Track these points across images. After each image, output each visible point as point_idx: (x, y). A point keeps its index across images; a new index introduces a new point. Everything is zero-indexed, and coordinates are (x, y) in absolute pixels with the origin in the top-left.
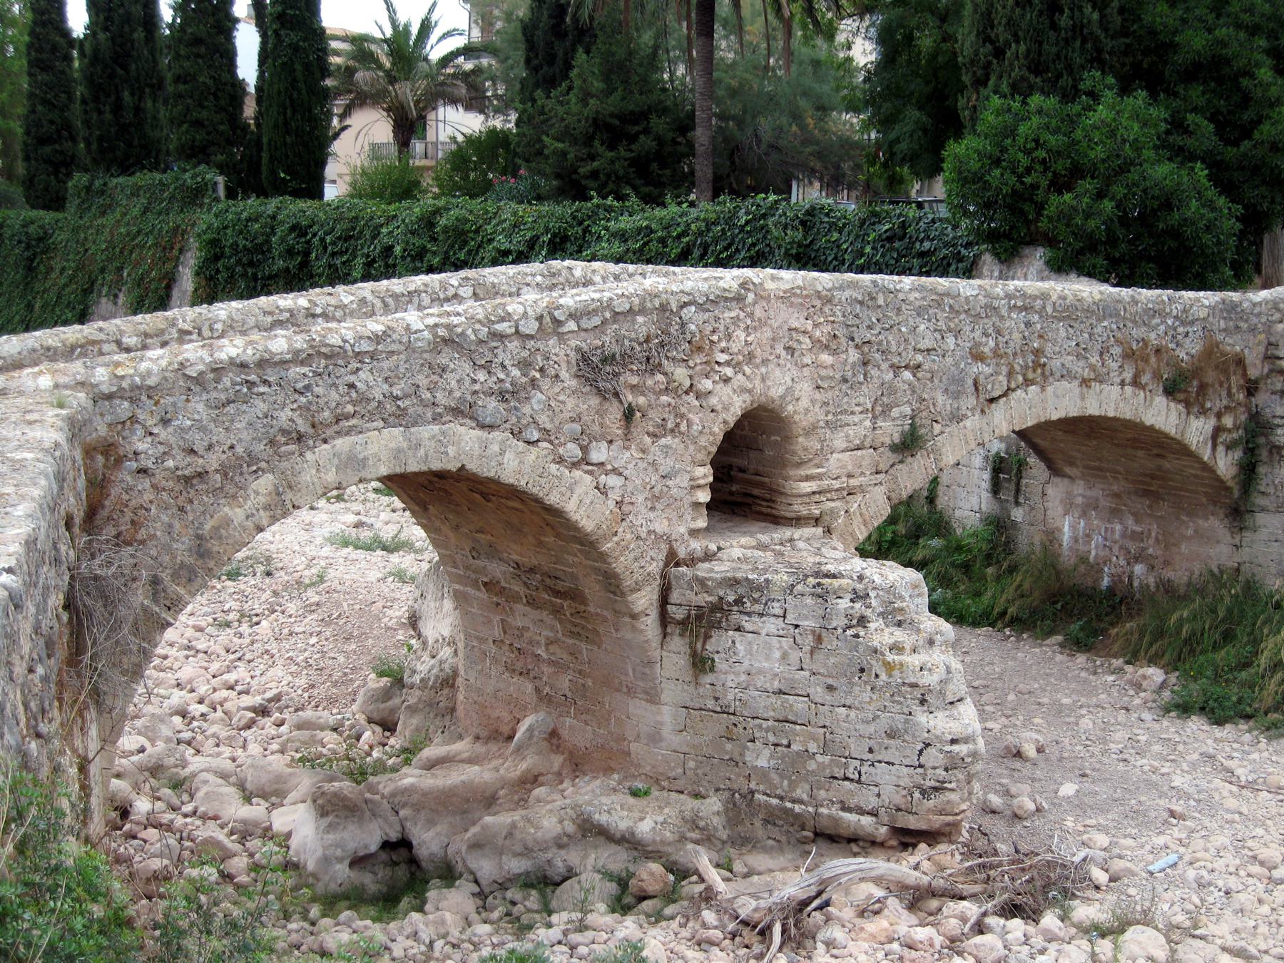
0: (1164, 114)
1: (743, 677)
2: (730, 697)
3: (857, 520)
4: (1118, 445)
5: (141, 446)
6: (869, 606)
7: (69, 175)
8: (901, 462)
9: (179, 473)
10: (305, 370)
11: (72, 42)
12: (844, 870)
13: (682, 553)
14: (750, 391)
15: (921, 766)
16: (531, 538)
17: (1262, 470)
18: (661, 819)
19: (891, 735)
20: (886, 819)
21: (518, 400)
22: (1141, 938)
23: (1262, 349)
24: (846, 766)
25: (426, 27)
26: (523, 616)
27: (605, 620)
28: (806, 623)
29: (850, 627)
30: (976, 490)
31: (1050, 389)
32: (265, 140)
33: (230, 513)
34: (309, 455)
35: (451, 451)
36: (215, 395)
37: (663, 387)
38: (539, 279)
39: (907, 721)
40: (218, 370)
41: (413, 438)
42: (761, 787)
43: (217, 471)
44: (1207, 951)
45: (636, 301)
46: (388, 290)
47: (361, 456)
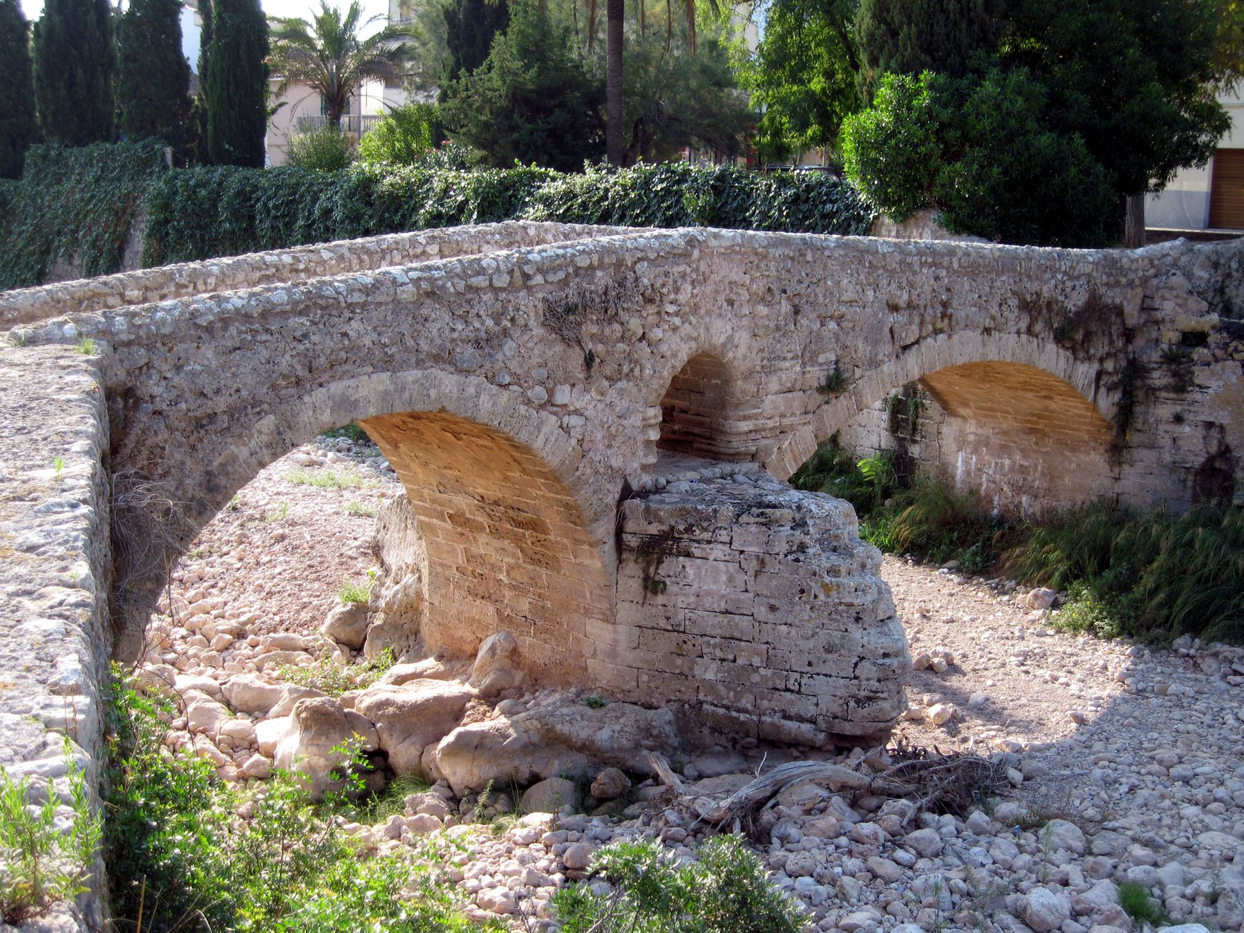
0: (1045, 90)
1: (692, 599)
2: (681, 617)
3: (788, 458)
4: (1009, 388)
5: (156, 390)
6: (807, 534)
7: (25, 147)
8: (827, 403)
9: (191, 414)
10: (303, 320)
11: (26, 25)
12: (795, 772)
13: (635, 485)
14: (695, 339)
15: (856, 678)
16: (497, 473)
17: (1138, 409)
18: (617, 728)
19: (829, 650)
20: (823, 726)
21: (492, 347)
22: (1061, 830)
23: (1138, 301)
24: (787, 678)
25: (354, 14)
26: (485, 545)
27: (565, 547)
28: (751, 549)
29: (791, 553)
30: (875, 429)
31: (956, 337)
32: (210, 114)
33: (236, 451)
34: (306, 399)
35: (433, 393)
36: (223, 343)
37: (619, 335)
38: (497, 237)
39: (843, 637)
40: (225, 320)
41: (399, 381)
42: (709, 698)
43: (224, 412)
44: (1120, 841)
46: (363, 247)
47: (353, 399)
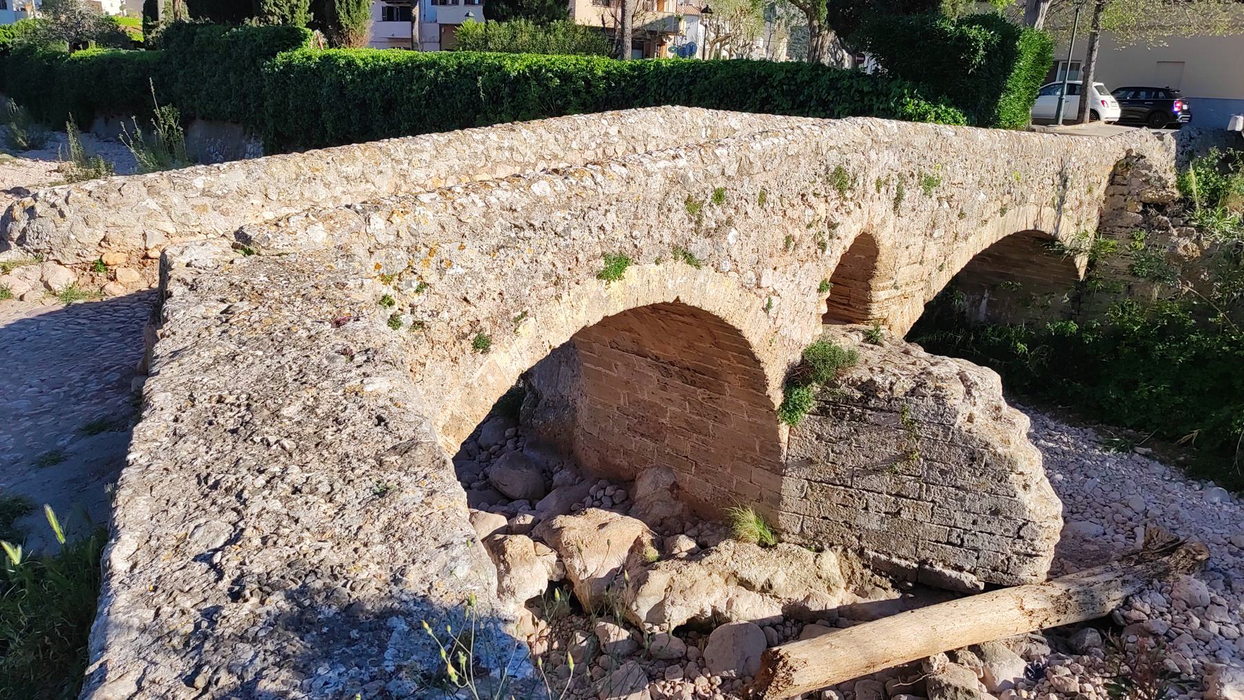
10: (565, 213)
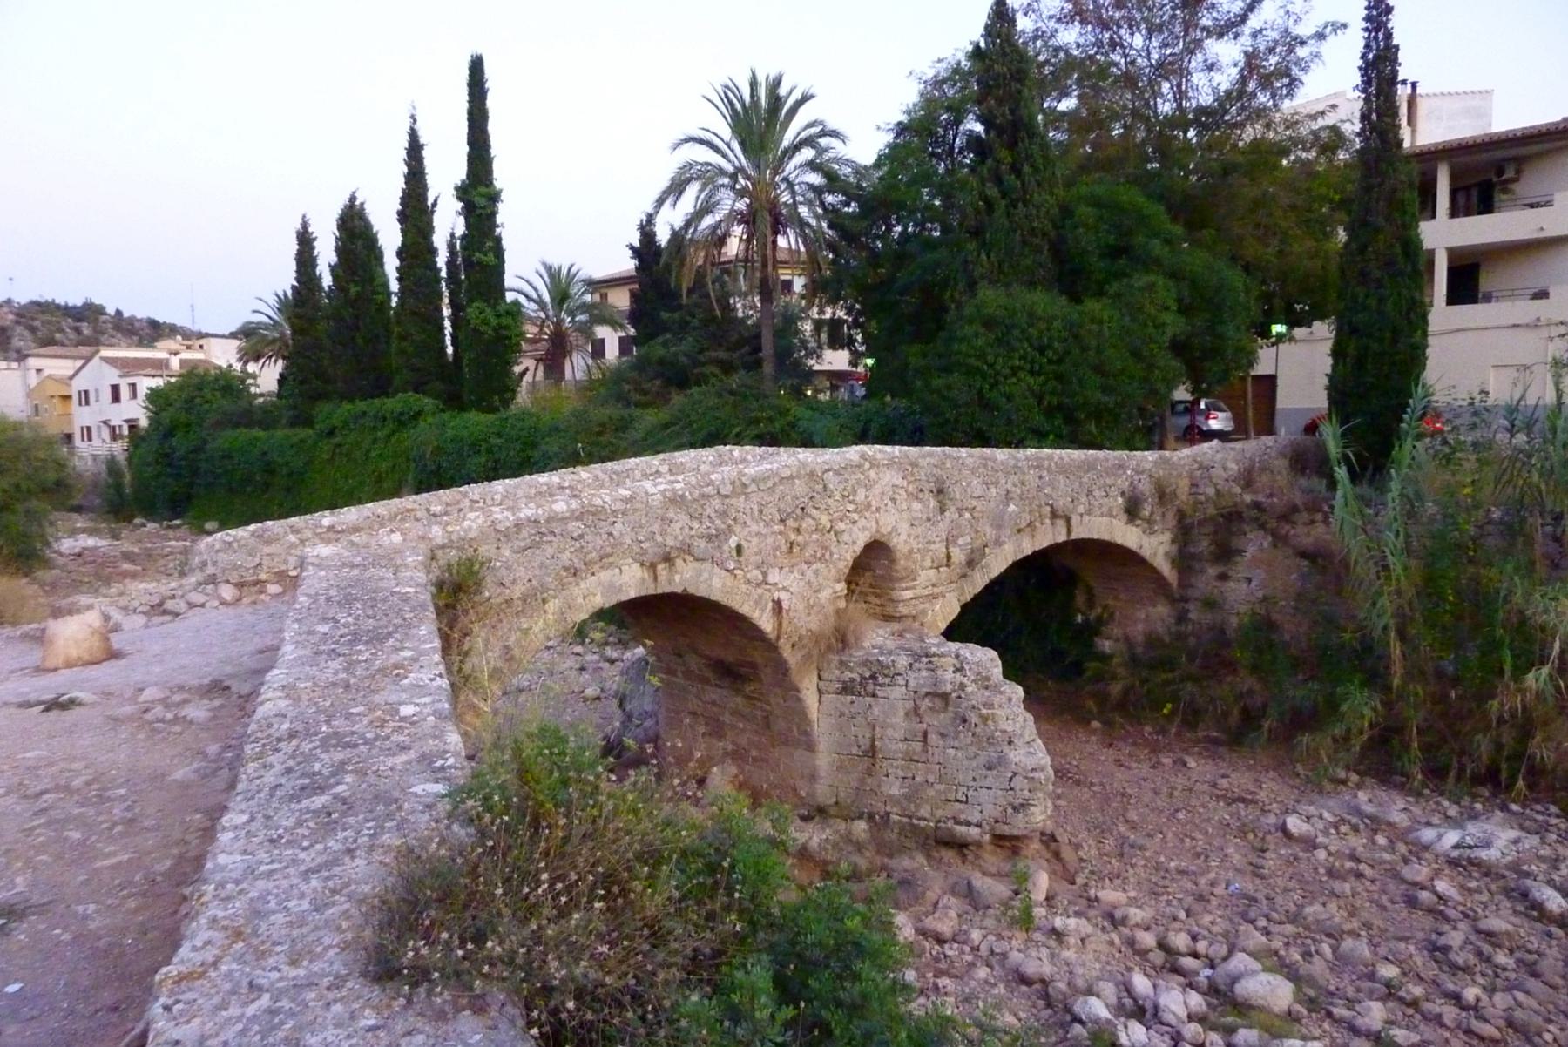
10: (579, 524)
11: (391, 308)
36: (518, 543)
42: (895, 810)
43: (519, 598)
45: (795, 470)
